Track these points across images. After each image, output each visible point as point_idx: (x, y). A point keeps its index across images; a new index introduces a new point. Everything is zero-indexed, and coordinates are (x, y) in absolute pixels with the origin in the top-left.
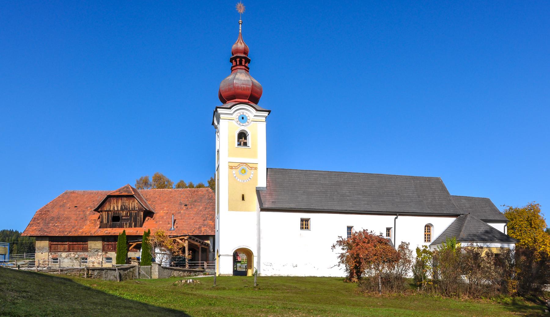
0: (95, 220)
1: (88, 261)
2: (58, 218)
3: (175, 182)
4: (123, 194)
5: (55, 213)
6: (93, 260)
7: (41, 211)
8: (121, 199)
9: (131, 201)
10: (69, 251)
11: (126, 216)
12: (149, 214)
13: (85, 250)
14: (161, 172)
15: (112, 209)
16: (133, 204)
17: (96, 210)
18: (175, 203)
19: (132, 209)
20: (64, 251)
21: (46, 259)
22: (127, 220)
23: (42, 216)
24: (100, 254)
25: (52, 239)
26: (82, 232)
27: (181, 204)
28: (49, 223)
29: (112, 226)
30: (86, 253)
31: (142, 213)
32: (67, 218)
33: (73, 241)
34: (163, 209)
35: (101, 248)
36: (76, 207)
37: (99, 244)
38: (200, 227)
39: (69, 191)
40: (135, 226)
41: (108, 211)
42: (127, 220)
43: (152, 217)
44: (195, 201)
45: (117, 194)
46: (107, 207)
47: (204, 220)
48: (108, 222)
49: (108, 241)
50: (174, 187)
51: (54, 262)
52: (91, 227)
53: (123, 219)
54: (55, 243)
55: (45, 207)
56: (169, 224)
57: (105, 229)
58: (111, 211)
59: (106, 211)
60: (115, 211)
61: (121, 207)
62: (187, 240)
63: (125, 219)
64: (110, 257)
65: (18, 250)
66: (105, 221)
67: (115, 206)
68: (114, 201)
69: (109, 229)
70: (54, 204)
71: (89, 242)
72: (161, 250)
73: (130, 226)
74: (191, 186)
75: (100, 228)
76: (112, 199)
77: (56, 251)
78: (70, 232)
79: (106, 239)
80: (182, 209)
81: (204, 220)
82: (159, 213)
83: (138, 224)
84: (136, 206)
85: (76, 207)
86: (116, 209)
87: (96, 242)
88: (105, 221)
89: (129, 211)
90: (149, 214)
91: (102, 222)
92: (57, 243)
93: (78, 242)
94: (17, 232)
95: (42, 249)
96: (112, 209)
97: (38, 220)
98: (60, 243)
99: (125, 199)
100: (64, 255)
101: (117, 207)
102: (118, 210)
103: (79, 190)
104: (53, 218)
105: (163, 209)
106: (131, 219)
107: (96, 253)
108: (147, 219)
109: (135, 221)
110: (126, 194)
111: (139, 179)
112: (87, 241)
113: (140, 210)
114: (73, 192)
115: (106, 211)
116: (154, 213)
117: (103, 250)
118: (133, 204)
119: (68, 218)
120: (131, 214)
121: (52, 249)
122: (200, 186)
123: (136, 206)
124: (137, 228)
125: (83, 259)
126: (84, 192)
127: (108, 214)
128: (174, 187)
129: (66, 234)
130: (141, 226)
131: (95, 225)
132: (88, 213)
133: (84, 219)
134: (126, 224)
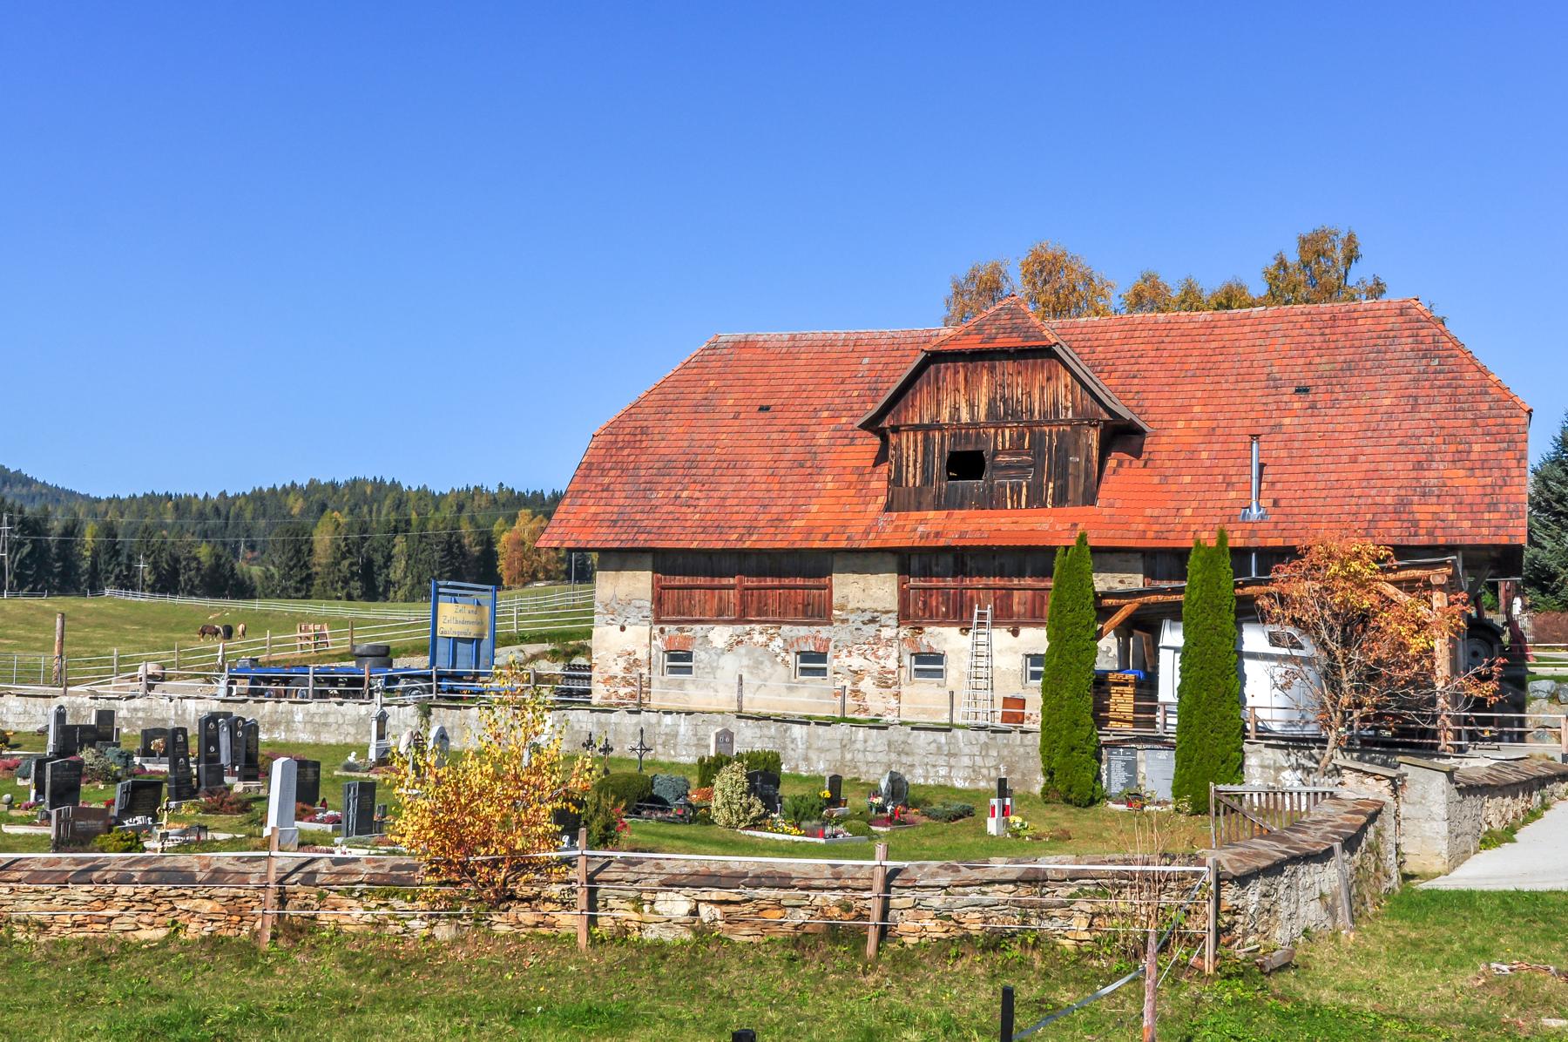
0: (860, 472)
1: (832, 664)
2: (692, 464)
3: (1119, 282)
4: (1002, 342)
5: (671, 439)
6: (857, 662)
7: (614, 428)
8: (992, 370)
9: (1040, 377)
10: (742, 619)
11: (1017, 448)
12: (1122, 435)
13: (820, 613)
14: (1054, 244)
15: (945, 416)
16: (1045, 393)
17: (872, 425)
18: (1241, 377)
19: (1043, 413)
20: (720, 617)
21: (642, 655)
22: (1021, 468)
23: (619, 449)
24: (887, 633)
25: (665, 561)
26: (809, 532)
27: (1274, 384)
28: (651, 486)
29: (946, 503)
30: (824, 632)
31: (1093, 437)
32: (732, 465)
33: (761, 573)
34: (1185, 409)
35: (894, 605)
36: (763, 409)
37: (881, 590)
38: (1402, 504)
39: (726, 336)
40: (1061, 499)
41: (926, 429)
42: (1021, 468)
43: (1138, 457)
44: (1349, 367)
45: (973, 343)
46: (920, 410)
47: (1418, 467)
48: (927, 479)
49: (926, 573)
50: (1115, 302)
51: (673, 670)
52: (841, 500)
53: (996, 467)
54: (678, 580)
55: (628, 413)
56: (1229, 485)
57: (915, 515)
58: (940, 428)
59: (915, 428)
60: (960, 426)
61: (992, 403)
62: (1441, 588)
63: (1009, 466)
64: (938, 648)
65: (410, 557)
66: (913, 477)
67: (963, 403)
68: (950, 375)
69: (931, 514)
70: (666, 398)
71: (837, 579)
72: (1275, 640)
73: (1036, 500)
74: (1191, 299)
75: (888, 508)
76: (947, 371)
77: (684, 616)
78: (750, 530)
79: (915, 564)
80: (1285, 410)
81: (1418, 467)
82: (1169, 433)
83: (1076, 488)
84: (1065, 401)
85: (763, 409)
86: (965, 417)
87: (871, 578)
88: (913, 477)
89: (1030, 425)
90: (1122, 435)
91: (896, 481)
92: (687, 580)
93: (778, 578)
94: (395, 486)
95: (619, 611)
96: (945, 416)
97: (604, 472)
98: (701, 581)
99: (1010, 366)
100: (720, 635)
101: (971, 406)
102: (974, 424)
103: (773, 332)
104: (667, 467)
105: (1185, 409)
106: (1036, 465)
107: (870, 630)
108: (1111, 463)
109: (1061, 471)
110: (1015, 342)
111: (962, 273)
112: (828, 572)
113: (1084, 420)
114: (746, 344)
115: (915, 428)
116: (1141, 432)
117: (904, 617)
118: (1045, 393)
119: (732, 465)
120: (1037, 441)
121: (668, 606)
122: (1228, 300)
123: (1065, 401)
124: (1069, 510)
125: (805, 656)
126: (793, 338)
127: (926, 439)
128: (1115, 302)
129: (732, 540)
130: (1090, 498)
131: (865, 497)
132: (822, 437)
133: (808, 466)
134: (1016, 490)
